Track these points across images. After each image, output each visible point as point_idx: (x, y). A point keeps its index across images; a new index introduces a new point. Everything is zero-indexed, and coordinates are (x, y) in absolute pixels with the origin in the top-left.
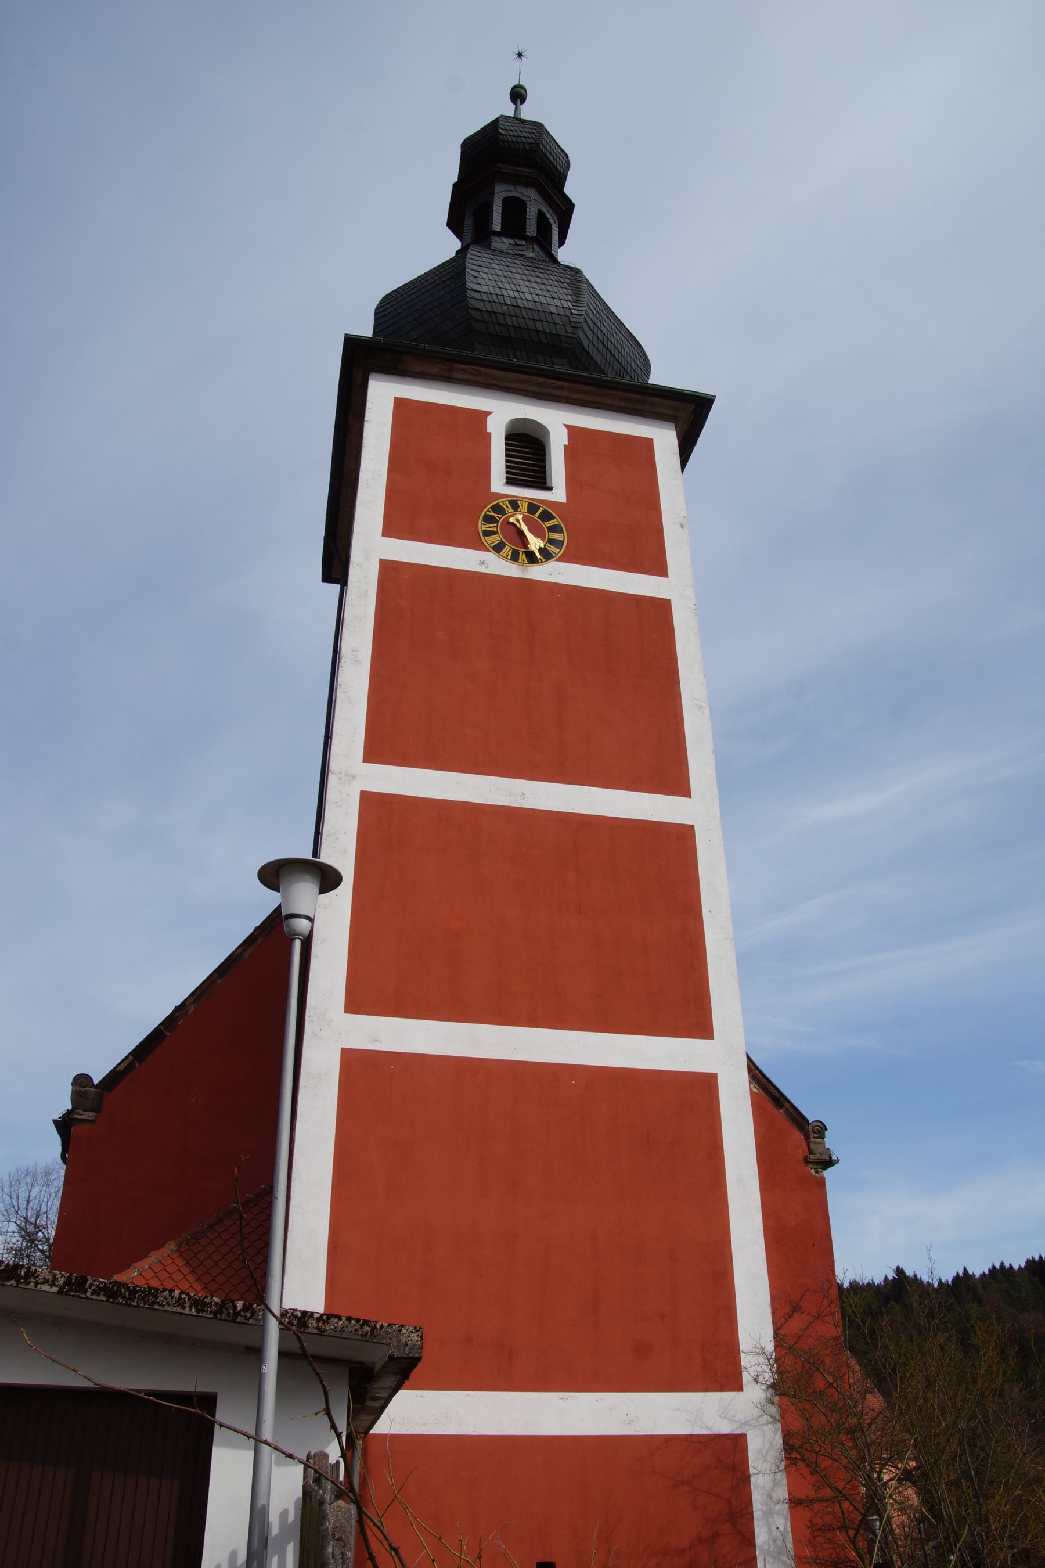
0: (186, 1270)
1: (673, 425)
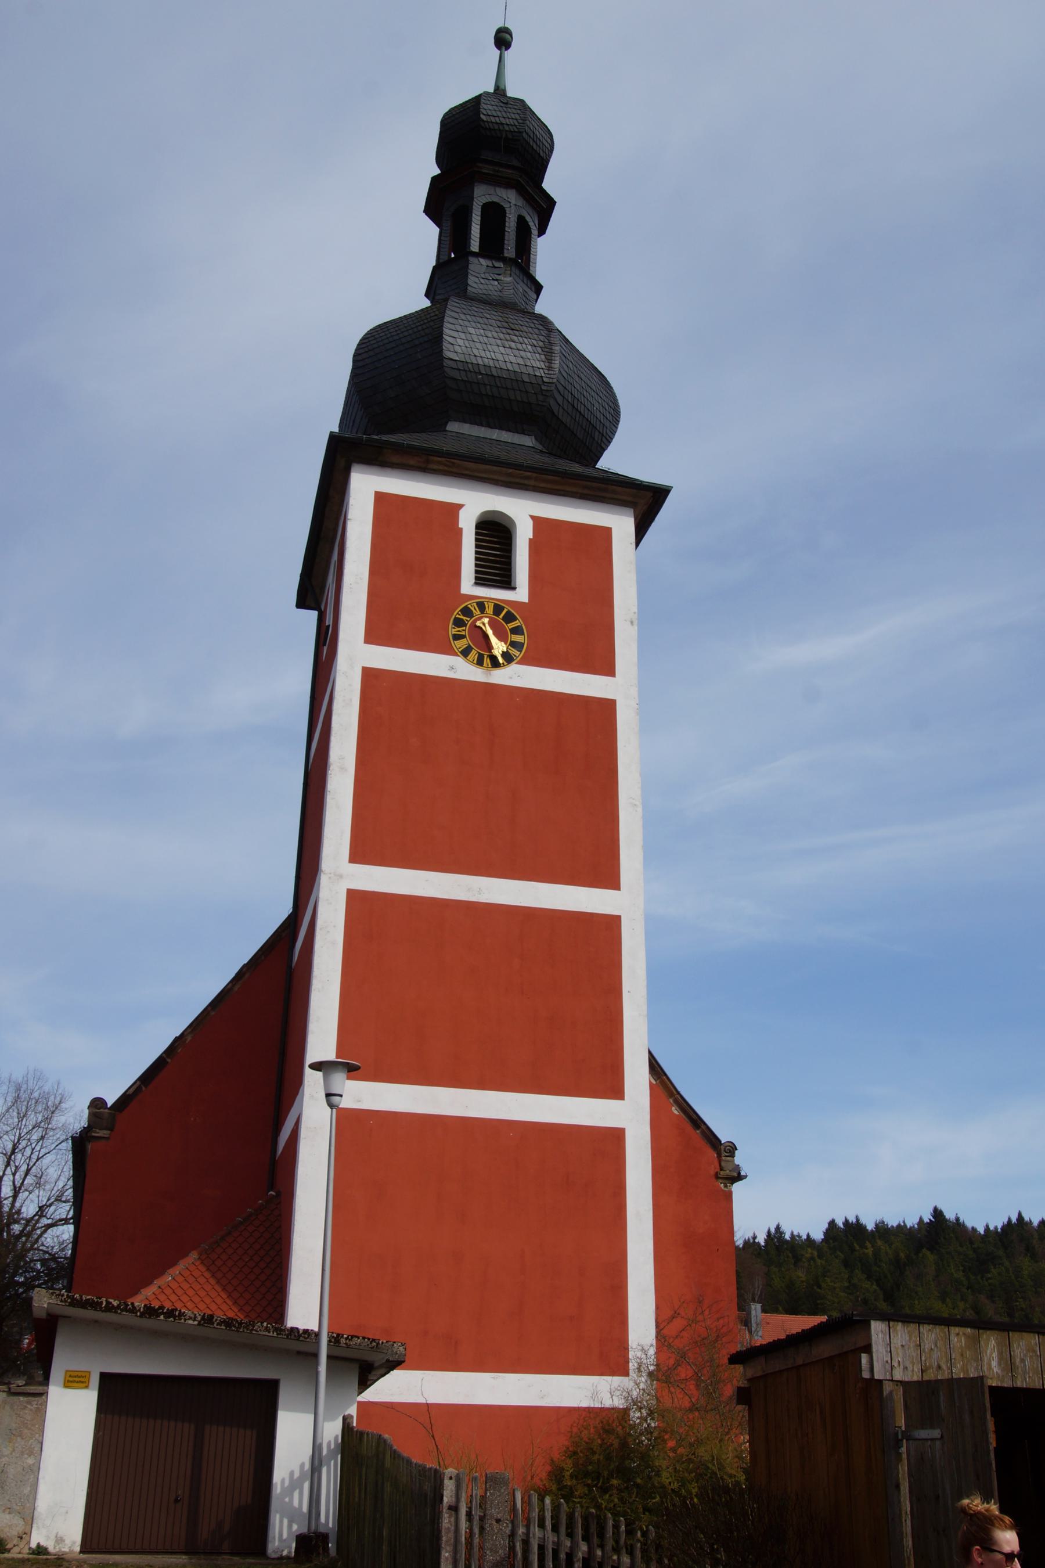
0: (208, 1275)
1: (632, 510)
